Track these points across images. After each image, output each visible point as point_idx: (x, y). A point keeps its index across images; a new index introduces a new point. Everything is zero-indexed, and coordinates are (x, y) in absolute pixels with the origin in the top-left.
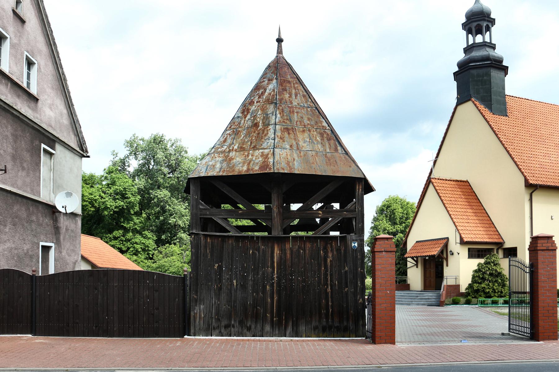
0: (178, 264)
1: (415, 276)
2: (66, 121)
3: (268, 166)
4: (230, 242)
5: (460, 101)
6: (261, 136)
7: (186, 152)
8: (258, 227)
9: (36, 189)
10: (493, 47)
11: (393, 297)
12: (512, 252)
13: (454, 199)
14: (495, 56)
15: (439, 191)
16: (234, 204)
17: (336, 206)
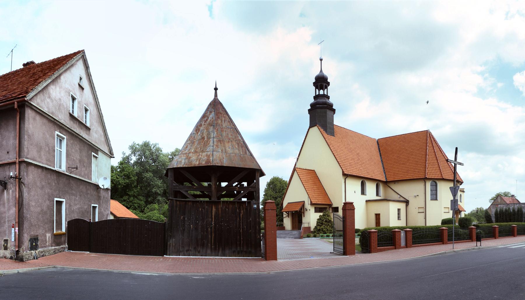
0: (157, 215)
1: (287, 222)
2: (103, 139)
3: (210, 161)
6: (206, 144)
7: (161, 151)
8: (204, 196)
9: (89, 175)
11: (275, 234)
12: (336, 209)
16: (191, 182)
17: (245, 184)
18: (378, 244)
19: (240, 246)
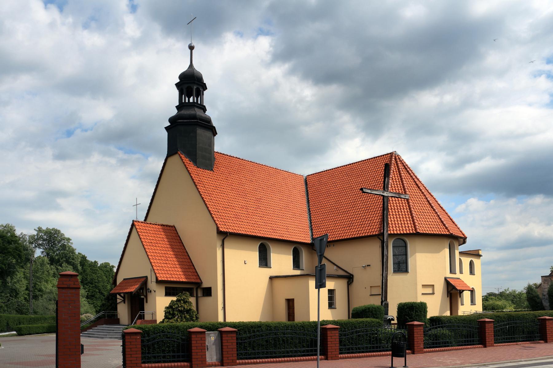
13: (155, 241)
14: (202, 116)
15: (140, 233)
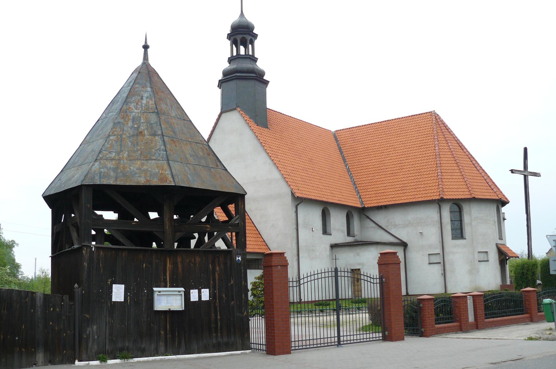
4: (124, 255)
5: (225, 109)
10: (255, 60)
18: (486, 315)
19: (216, 332)
